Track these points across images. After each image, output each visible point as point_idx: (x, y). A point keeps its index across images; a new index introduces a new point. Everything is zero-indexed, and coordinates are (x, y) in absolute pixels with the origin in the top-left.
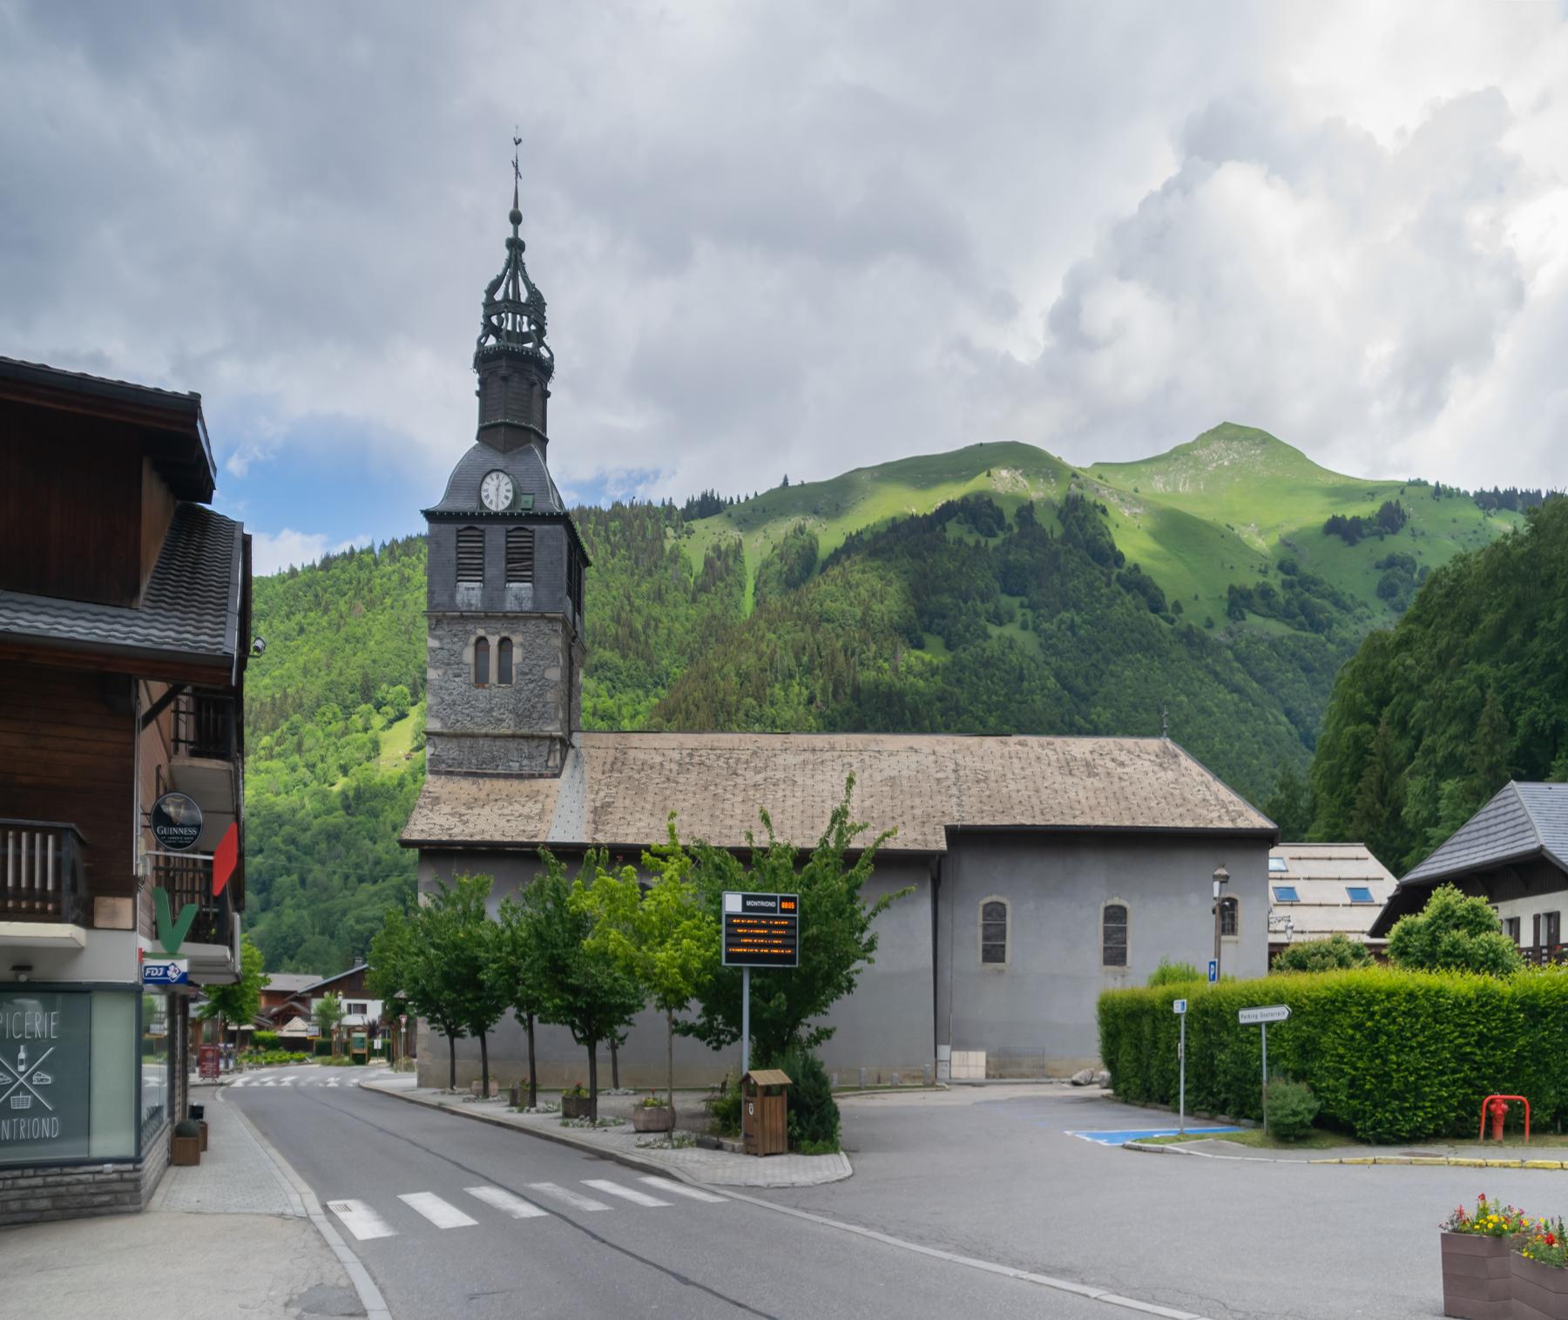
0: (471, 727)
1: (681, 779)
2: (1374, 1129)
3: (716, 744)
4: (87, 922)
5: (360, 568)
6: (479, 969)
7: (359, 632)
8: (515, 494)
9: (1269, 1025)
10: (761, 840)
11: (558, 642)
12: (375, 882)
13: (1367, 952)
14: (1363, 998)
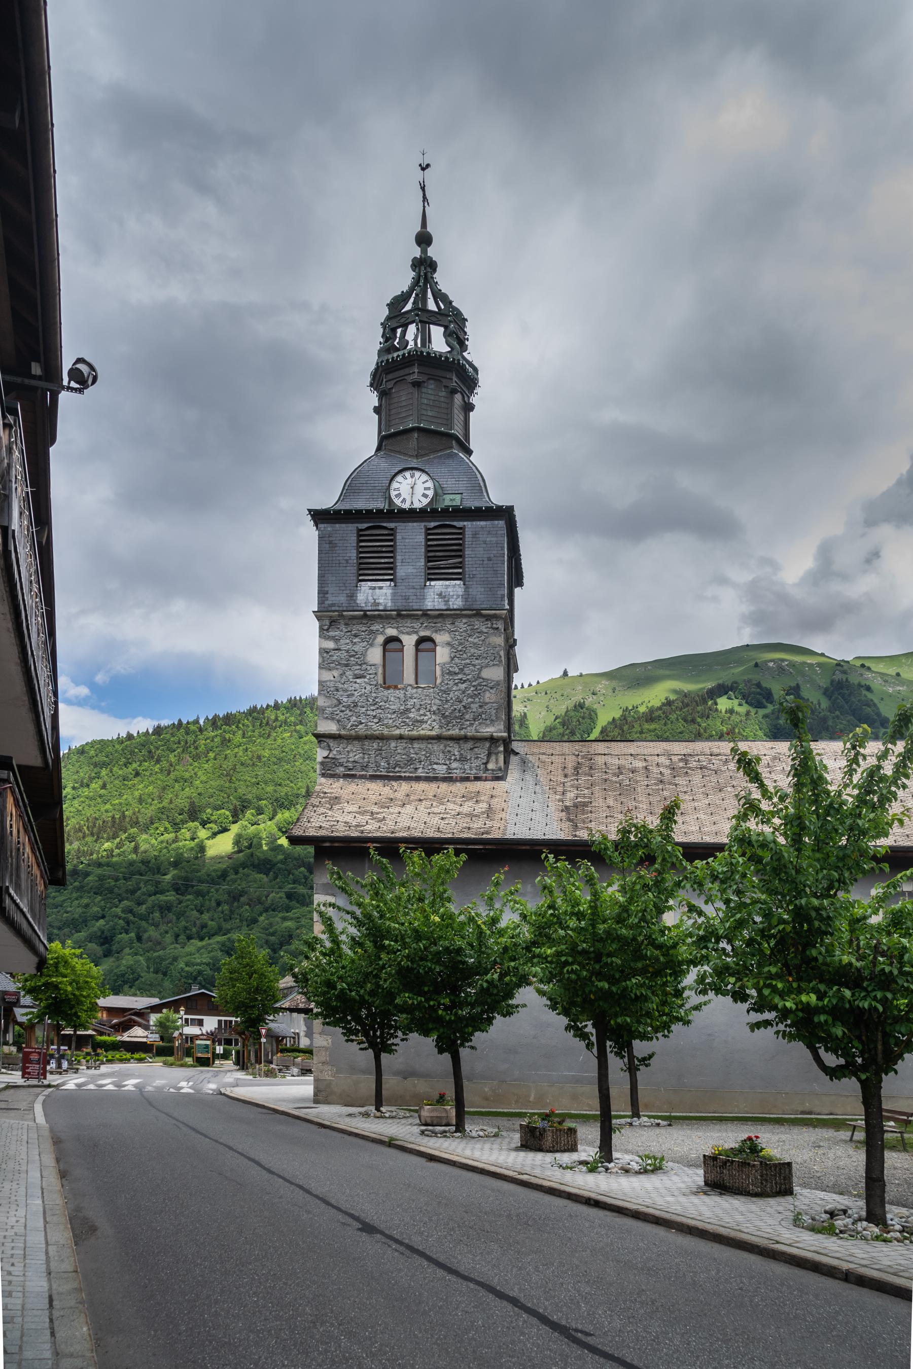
0: (376, 728)
3: (716, 751)
5: (187, 734)
7: (187, 775)
12: (202, 939)
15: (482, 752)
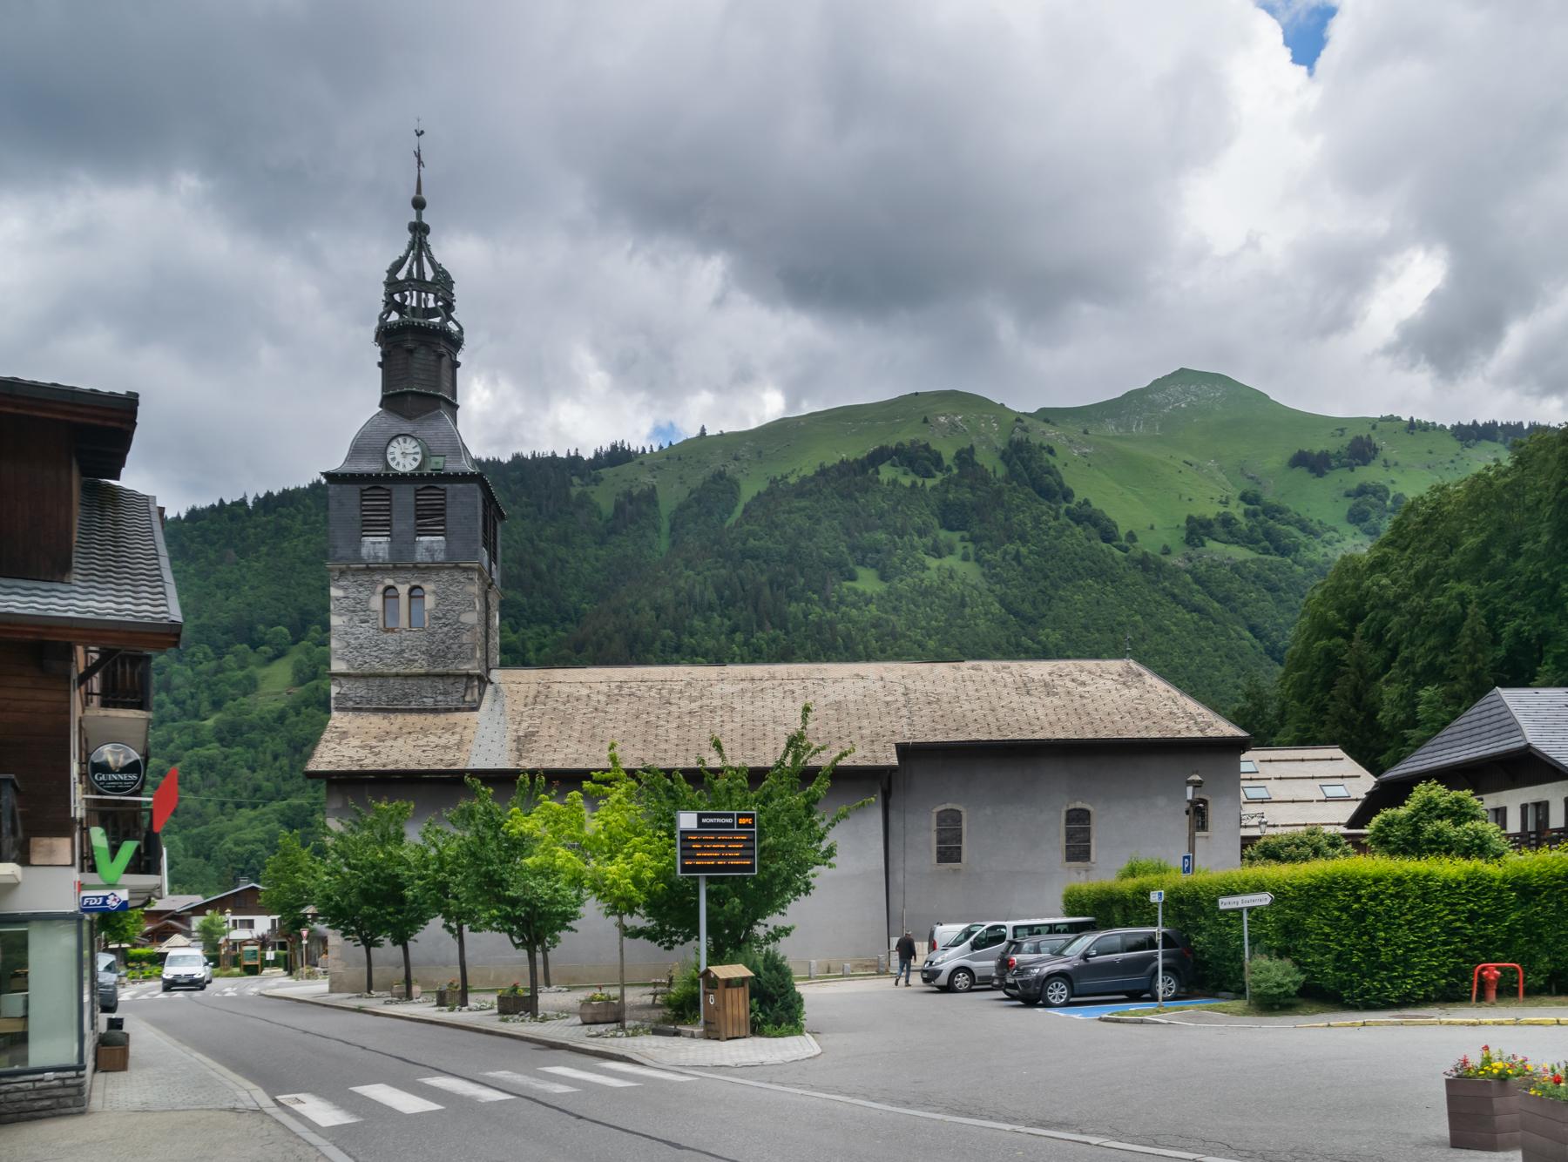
0: (379, 667)
1: (611, 709)
2: (1361, 996)
3: (646, 677)
4: (24, 861)
6: (403, 887)
8: (424, 457)
9: (1250, 910)
10: (715, 762)
11: (475, 589)
13: (1344, 841)
14: (1352, 885)
15: (461, 687)
